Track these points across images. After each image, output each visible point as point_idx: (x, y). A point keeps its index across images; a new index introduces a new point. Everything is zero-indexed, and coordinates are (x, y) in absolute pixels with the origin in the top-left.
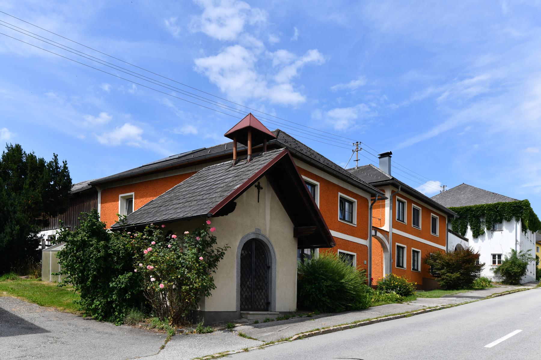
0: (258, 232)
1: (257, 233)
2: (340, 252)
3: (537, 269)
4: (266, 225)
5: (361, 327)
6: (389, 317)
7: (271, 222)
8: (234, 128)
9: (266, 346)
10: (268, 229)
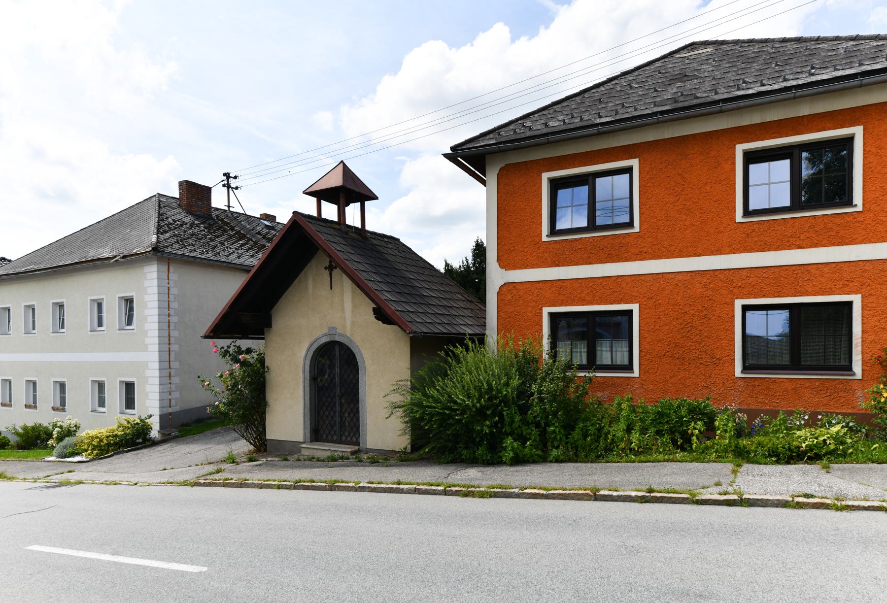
0: (332, 330)
2: (746, 308)
4: (345, 319)
5: (301, 491)
6: (434, 488)
7: (353, 311)
8: (312, 187)
10: (348, 324)
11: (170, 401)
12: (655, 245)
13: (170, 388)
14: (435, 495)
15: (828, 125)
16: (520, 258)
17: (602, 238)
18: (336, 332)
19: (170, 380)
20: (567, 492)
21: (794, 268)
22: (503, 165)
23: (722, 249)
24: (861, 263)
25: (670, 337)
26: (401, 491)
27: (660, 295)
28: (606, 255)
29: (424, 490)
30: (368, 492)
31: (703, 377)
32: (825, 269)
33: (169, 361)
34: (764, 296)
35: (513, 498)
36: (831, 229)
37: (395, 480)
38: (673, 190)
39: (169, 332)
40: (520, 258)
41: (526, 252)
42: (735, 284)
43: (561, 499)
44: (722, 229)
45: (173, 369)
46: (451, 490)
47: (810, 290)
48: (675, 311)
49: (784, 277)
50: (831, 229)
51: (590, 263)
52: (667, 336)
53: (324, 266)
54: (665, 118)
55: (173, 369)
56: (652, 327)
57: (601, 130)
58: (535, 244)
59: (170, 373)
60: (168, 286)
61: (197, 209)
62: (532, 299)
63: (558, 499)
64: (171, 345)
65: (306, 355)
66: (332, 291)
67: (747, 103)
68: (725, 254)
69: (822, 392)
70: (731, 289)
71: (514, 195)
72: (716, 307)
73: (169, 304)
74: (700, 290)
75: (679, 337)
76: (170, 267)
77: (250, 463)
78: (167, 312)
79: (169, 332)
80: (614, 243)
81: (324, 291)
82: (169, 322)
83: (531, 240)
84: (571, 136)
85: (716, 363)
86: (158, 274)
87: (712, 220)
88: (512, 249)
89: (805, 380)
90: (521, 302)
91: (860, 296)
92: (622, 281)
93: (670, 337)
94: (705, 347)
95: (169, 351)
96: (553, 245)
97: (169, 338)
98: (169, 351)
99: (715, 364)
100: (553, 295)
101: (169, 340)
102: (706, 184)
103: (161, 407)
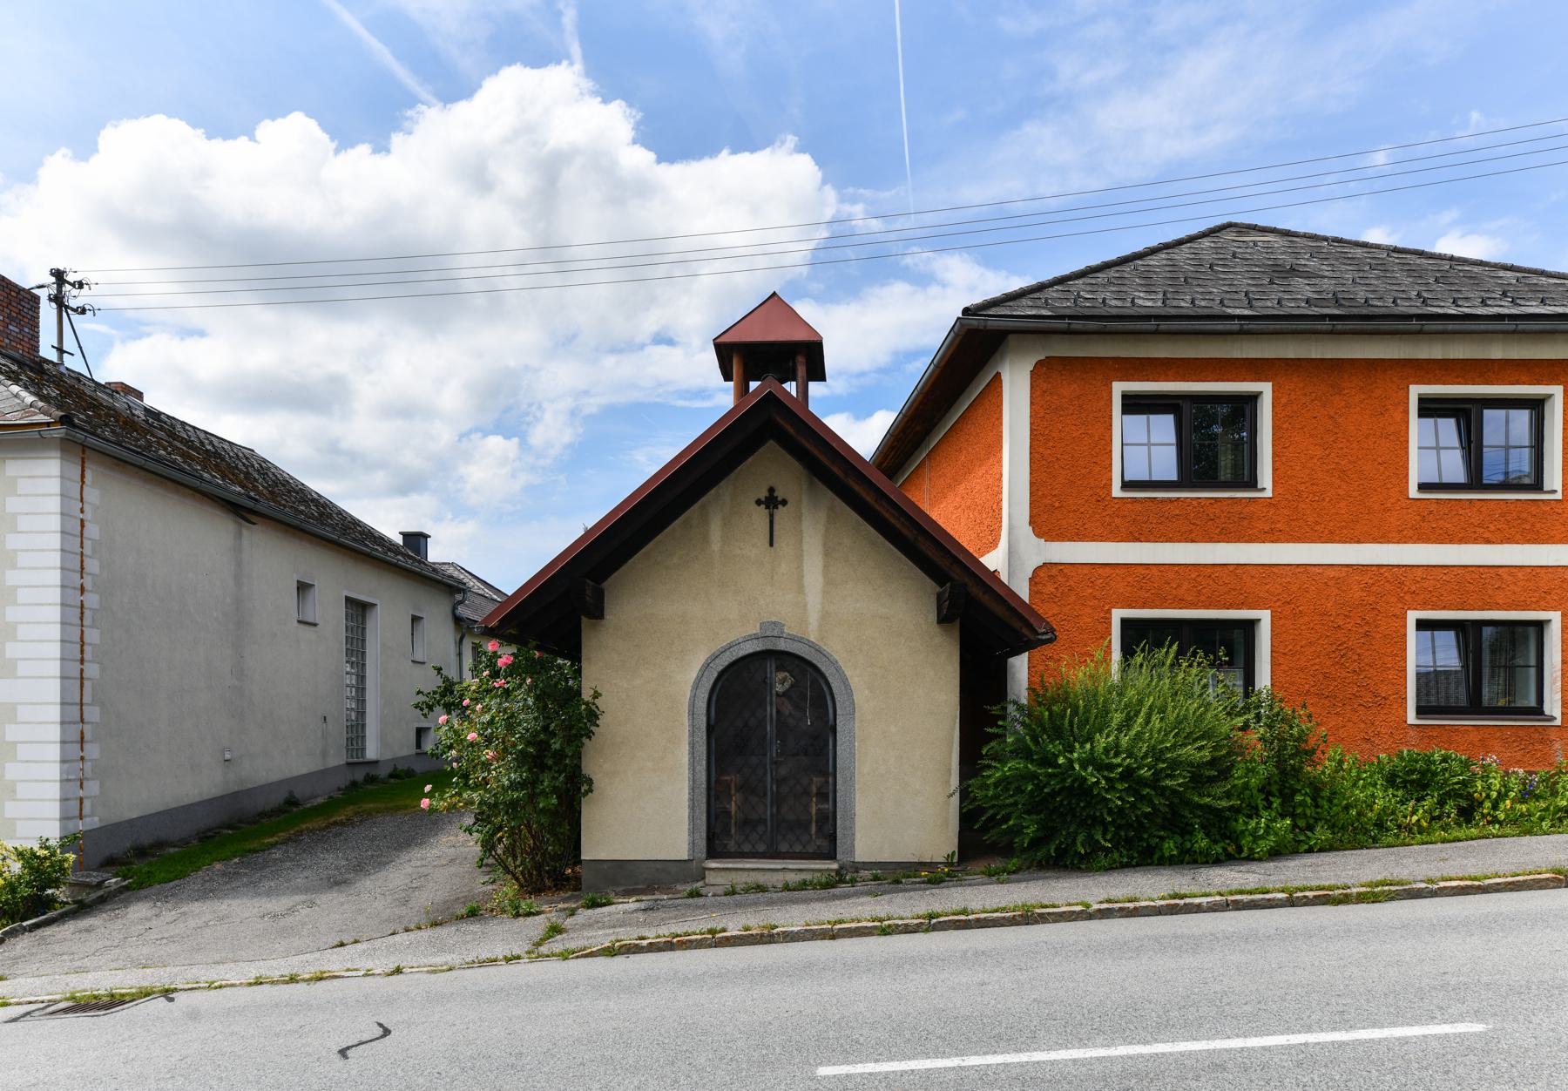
1: (768, 633)
2: (1422, 625)
3: (17, 659)
7: (825, 593)
9: (417, 970)
10: (813, 618)
11: (81, 803)
12: (1294, 520)
13: (82, 769)
14: (1269, 908)
15: (1523, 378)
16: (1071, 521)
17: (1213, 501)
18: (782, 632)
19: (82, 750)
20: (1520, 878)
21: (1481, 570)
22: (1043, 358)
23: (1390, 535)
24: (1560, 569)
25: (1315, 664)
26: (1195, 910)
27: (1301, 598)
28: (1219, 530)
29: (1247, 903)
30: (1120, 917)
31: (1363, 725)
32: (1520, 575)
33: (82, 705)
34: (1444, 608)
35: (1425, 897)
36: (1525, 520)
37: (1104, 896)
38: (1322, 438)
39: (82, 632)
40: (1071, 521)
41: (1082, 513)
42: (1406, 589)
43: (1511, 890)
44: (1389, 505)
45: (88, 723)
46: (1305, 897)
47: (1500, 602)
48: (1323, 624)
49: (1469, 583)
50: (1525, 520)
51: (1193, 541)
52: (1312, 662)
53: (756, 499)
54: (1345, 327)
55: (88, 723)
56: (1290, 647)
57: (1245, 327)
58: (1099, 501)
59: (82, 733)
60: (81, 516)
61: (7, 341)
62: (1092, 593)
63: (1506, 891)
64: (85, 664)
65: (699, 679)
66: (772, 548)
67: (1457, 327)
68: (1393, 543)
69: (1515, 744)
70: (1402, 595)
71: (1062, 413)
72: (1381, 620)
73: (82, 561)
74: (1359, 594)
75: (1329, 663)
76: (86, 465)
77: (876, 883)
78: (78, 583)
79: (82, 632)
80: (1232, 511)
81: (752, 544)
82: (82, 606)
83: (1091, 492)
84: (1197, 327)
85: (1380, 705)
86: (62, 484)
87: (1376, 491)
88: (1057, 505)
89: (1496, 729)
90: (1072, 598)
91: (1559, 613)
92: (1244, 573)
93: (1315, 664)
94: (1366, 679)
95: (82, 678)
96: (1130, 506)
97: (82, 646)
98: (82, 678)
99: (1380, 705)
100: (1129, 588)
101: (82, 652)
102: (1367, 437)
103: (64, 818)
